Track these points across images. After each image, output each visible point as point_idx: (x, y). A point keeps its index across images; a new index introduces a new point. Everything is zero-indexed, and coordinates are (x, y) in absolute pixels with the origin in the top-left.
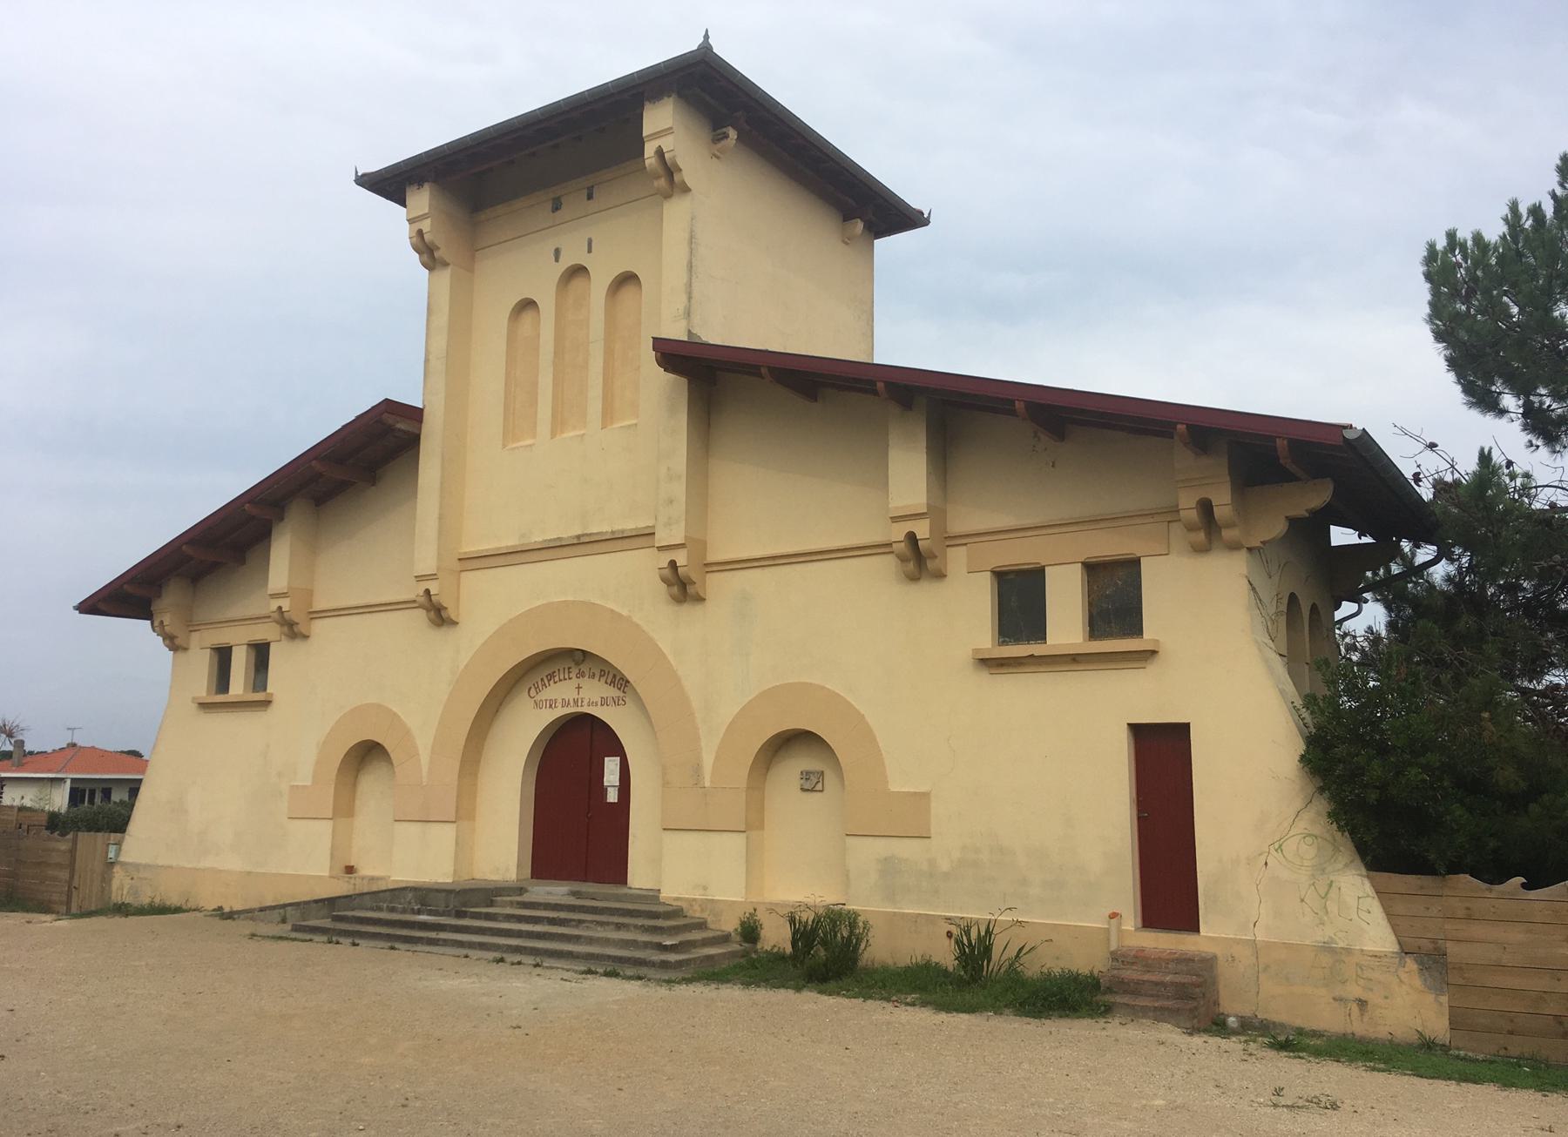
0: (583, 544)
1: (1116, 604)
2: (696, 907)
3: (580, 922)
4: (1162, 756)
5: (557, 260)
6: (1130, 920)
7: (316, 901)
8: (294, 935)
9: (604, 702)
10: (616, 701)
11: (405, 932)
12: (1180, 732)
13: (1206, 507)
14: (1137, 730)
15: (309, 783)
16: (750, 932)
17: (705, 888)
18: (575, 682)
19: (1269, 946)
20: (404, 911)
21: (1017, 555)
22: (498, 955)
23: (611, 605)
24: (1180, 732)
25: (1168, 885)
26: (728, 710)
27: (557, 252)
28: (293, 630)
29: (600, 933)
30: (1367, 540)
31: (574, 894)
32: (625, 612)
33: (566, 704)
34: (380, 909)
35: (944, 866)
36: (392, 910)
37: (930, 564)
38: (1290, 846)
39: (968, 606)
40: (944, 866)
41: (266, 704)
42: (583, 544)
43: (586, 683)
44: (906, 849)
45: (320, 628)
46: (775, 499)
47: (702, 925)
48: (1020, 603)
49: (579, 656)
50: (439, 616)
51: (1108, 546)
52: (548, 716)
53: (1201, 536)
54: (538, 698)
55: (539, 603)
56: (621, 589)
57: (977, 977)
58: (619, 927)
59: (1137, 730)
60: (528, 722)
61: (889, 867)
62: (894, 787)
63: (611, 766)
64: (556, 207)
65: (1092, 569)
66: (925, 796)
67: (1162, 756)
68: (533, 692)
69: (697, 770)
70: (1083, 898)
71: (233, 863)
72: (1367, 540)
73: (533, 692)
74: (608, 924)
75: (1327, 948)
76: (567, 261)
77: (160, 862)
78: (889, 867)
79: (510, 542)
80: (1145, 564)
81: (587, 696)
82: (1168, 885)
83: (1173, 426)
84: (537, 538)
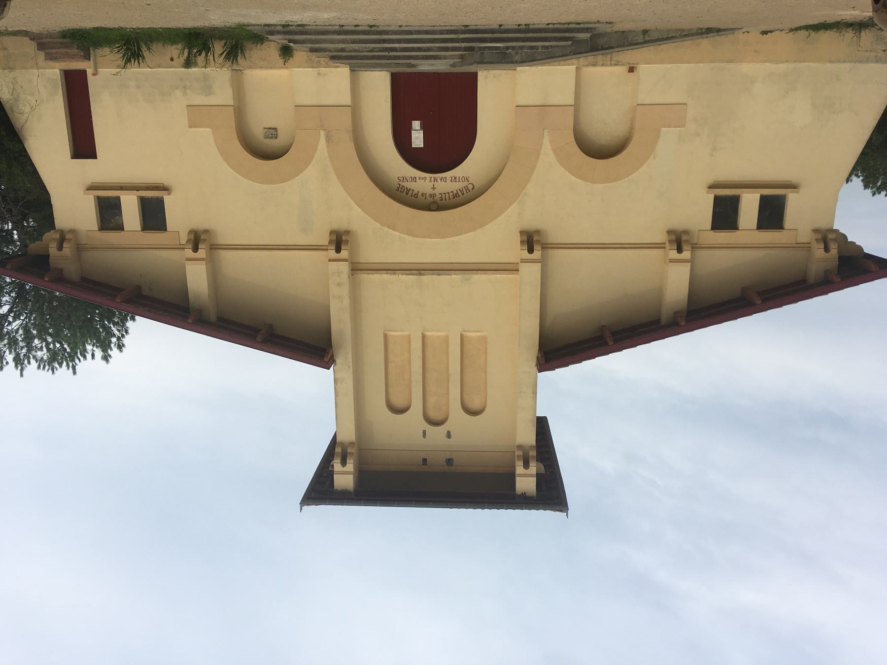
0: (419, 270)
1: (109, 212)
2: (324, 63)
3: (372, 51)
4: (83, 145)
5: (449, 433)
6: (89, 72)
7: (612, 48)
8: (591, 26)
9: (414, 179)
10: (404, 179)
11: (495, 35)
13: (60, 248)
14: (93, 156)
15: (664, 129)
16: (286, 52)
17: (319, 74)
18: (437, 192)
19: (32, 68)
20: (522, 48)
21: (154, 237)
22: (374, 29)
23: (397, 234)
25: (76, 90)
26: (311, 172)
27: (449, 435)
28: (679, 240)
29: (356, 46)
31: (413, 66)
32: (386, 229)
33: (444, 179)
34: (544, 47)
35: (178, 93)
36: (532, 48)
38: (28, 109)
39: (179, 215)
40: (178, 93)
41: (711, 187)
42: (419, 270)
43: (429, 191)
44: (199, 99)
46: (301, 279)
47: (312, 50)
48: (153, 214)
49: (434, 207)
50: (530, 240)
51: (112, 237)
53: (684, 238)
54: (465, 183)
55: (453, 239)
57: (133, 45)
58: (343, 50)
59: (93, 156)
60: (472, 168)
61: (208, 90)
62: (209, 130)
63: (418, 139)
64: (450, 461)
65: (121, 228)
66: (190, 127)
67: (83, 145)
68: (470, 187)
69: (328, 139)
70: (107, 80)
71: (747, 68)
72: (322, 144)
73: (470, 187)
74: (350, 51)
75: (11, 69)
76: (442, 430)
77: (847, 65)
78: (208, 90)
79: (477, 277)
80: (709, 226)
81: (424, 183)
82: (76, 90)
83: (511, 477)
84: (456, 277)
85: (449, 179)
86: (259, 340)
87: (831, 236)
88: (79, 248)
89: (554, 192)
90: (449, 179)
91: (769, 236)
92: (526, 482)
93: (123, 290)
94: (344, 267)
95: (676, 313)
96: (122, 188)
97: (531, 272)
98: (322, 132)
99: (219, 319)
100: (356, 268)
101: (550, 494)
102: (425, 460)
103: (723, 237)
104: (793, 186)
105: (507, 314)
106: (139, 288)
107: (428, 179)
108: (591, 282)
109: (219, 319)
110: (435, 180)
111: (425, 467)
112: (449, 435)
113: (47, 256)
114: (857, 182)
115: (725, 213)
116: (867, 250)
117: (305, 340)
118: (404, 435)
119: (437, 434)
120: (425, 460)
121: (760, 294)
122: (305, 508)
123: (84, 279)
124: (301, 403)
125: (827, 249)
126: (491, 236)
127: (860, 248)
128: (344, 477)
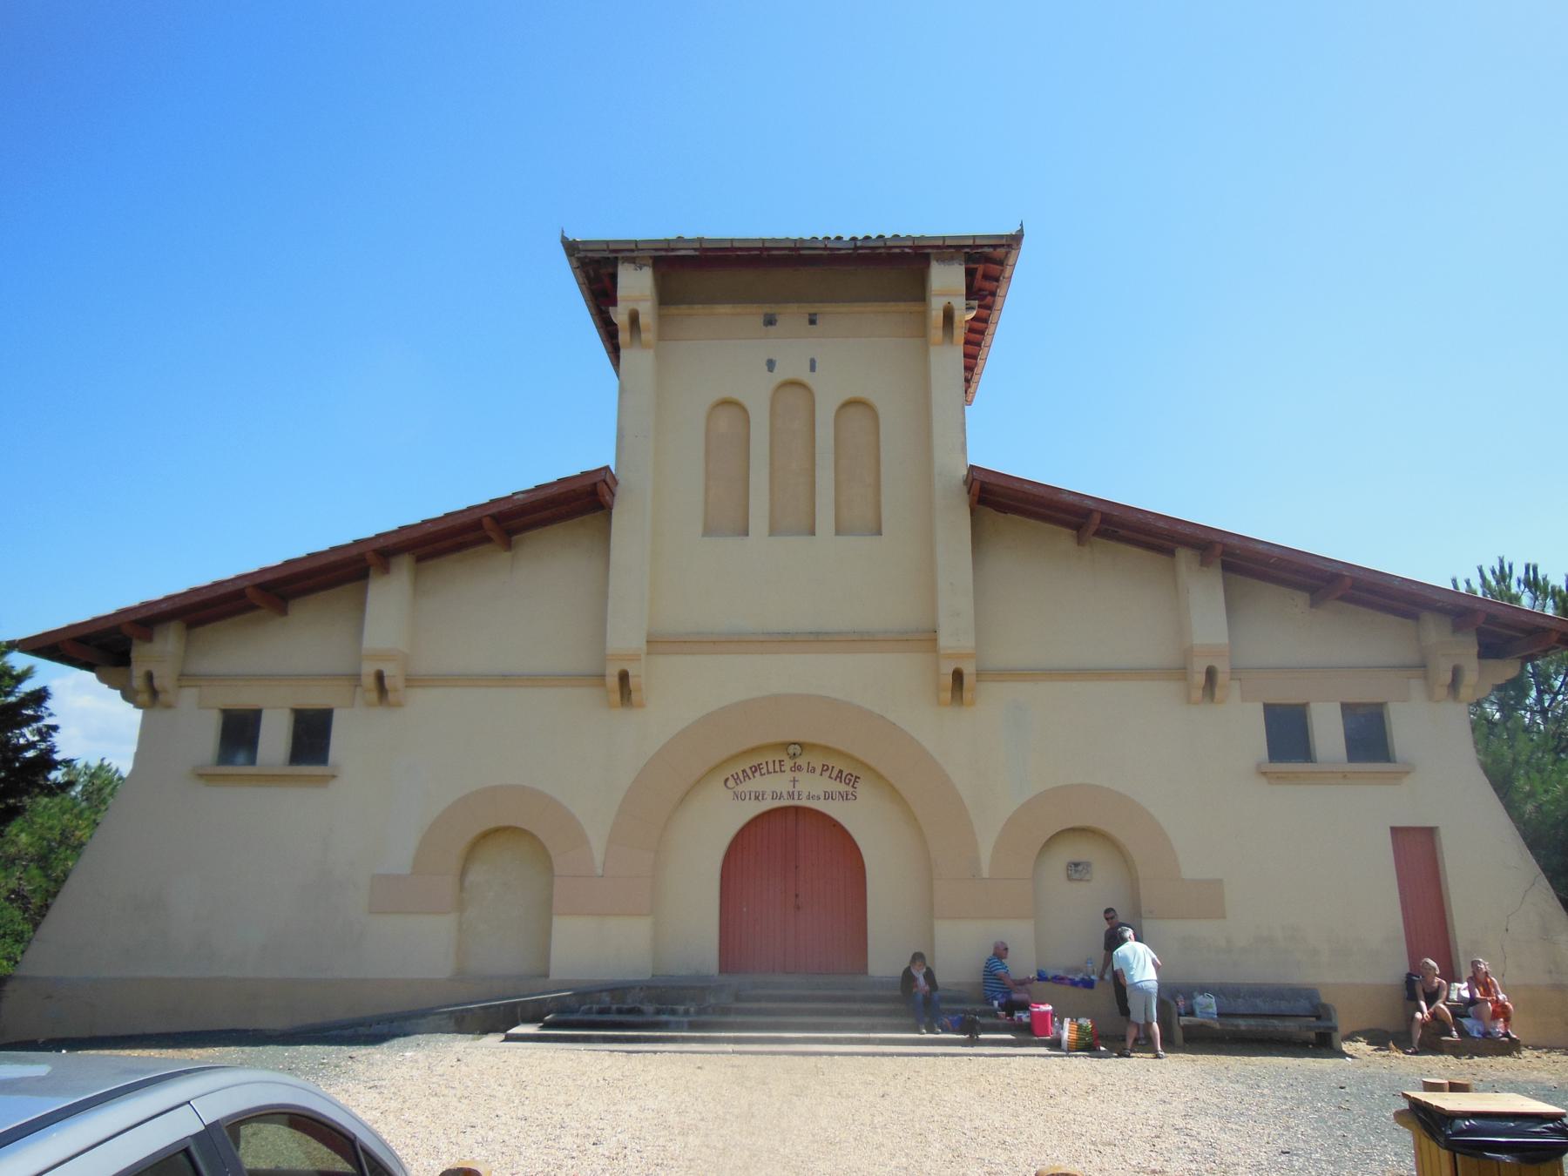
1: (1369, 738)
4: (1417, 852)
9: (828, 796)
10: (845, 797)
12: (1430, 833)
13: (1457, 673)
14: (1396, 831)
18: (789, 775)
24: (1430, 833)
27: (771, 365)
30: (986, 852)
37: (162, 697)
39: (1246, 728)
45: (421, 701)
48: (1288, 735)
52: (753, 809)
54: (740, 788)
56: (887, 688)
59: (1396, 831)
64: (770, 321)
67: (1417, 852)
68: (731, 783)
72: (986, 852)
73: (731, 783)
76: (780, 375)
83: (666, 297)
85: (768, 796)
86: (1097, 518)
87: (144, 697)
88: (1422, 667)
89: (583, 767)
90: (768, 796)
91: (243, 699)
92: (635, 285)
93: (1341, 598)
94: (945, 641)
95: (385, 569)
96: (1345, 776)
97: (625, 637)
98: (985, 873)
99: (1171, 553)
100: (927, 638)
101: (597, 270)
102: (812, 322)
103: (314, 699)
104: (203, 776)
105: (656, 559)
106: (1314, 604)
107: (804, 796)
108: (515, 609)
109: (1171, 553)
110: (791, 795)
111: (813, 311)
112: (771, 365)
113: (1482, 655)
114: (1405, 1105)
115: (311, 738)
116: (90, 677)
117: (998, 500)
118: (845, 357)
119: (792, 365)
120: (812, 322)
121: (252, 607)
122: (1010, 229)
123: (1415, 617)
124: (1031, 415)
125: (149, 677)
126: (685, 695)
127: (102, 679)
128: (947, 281)
